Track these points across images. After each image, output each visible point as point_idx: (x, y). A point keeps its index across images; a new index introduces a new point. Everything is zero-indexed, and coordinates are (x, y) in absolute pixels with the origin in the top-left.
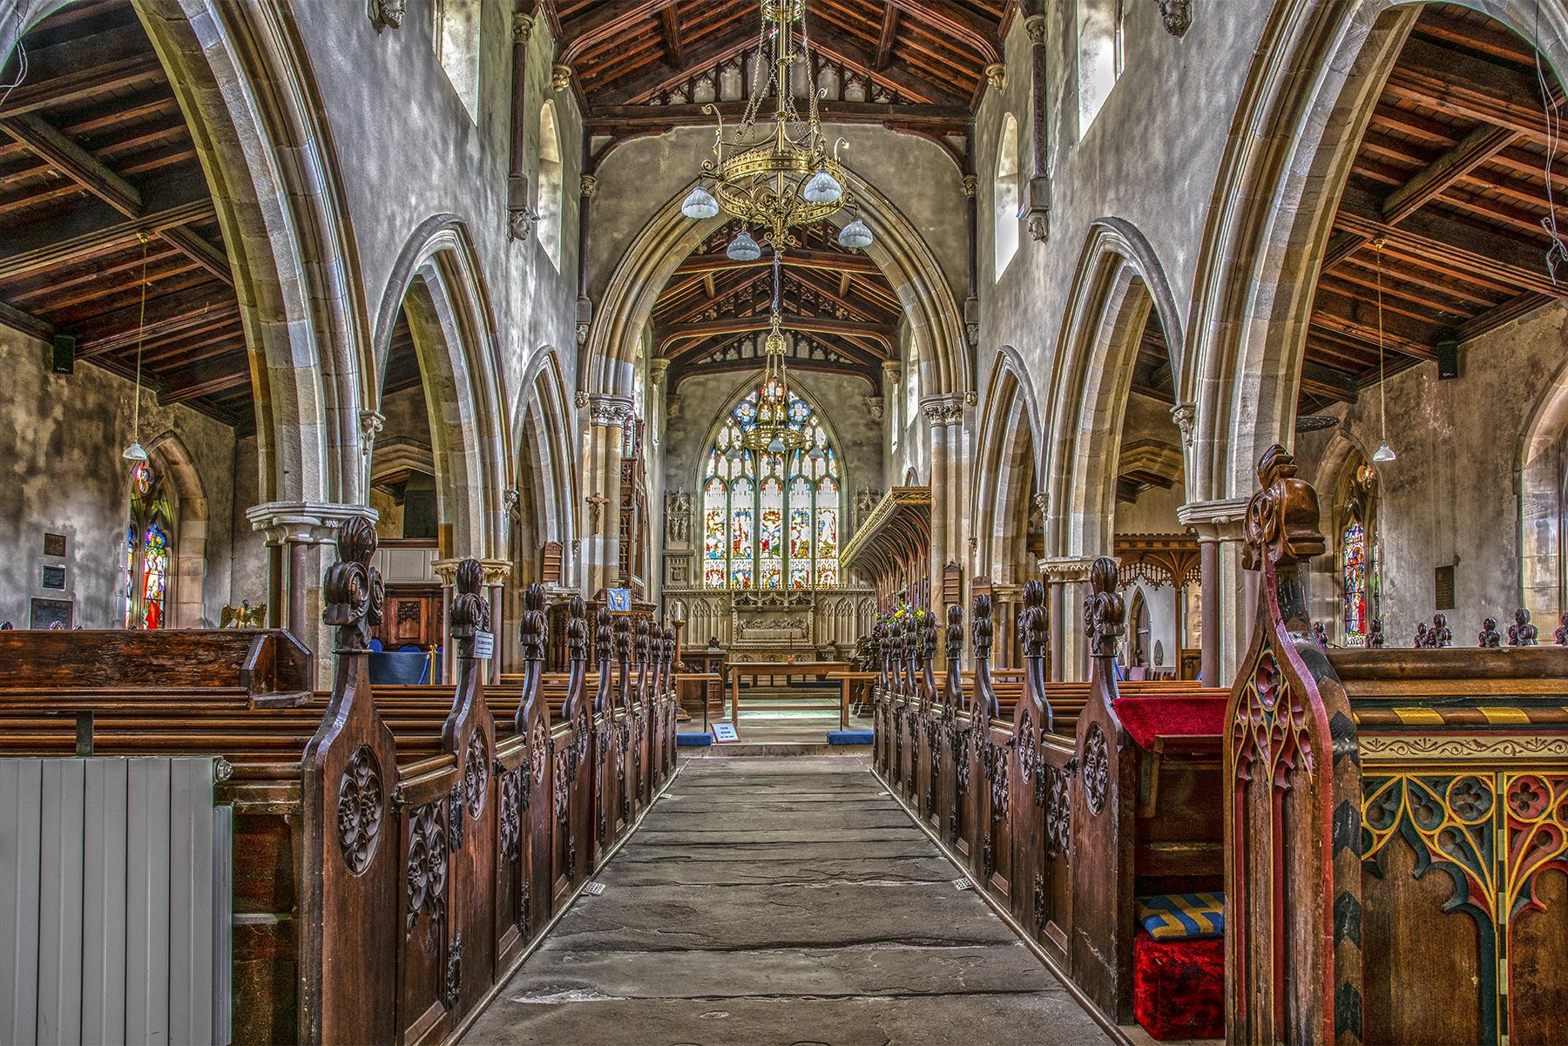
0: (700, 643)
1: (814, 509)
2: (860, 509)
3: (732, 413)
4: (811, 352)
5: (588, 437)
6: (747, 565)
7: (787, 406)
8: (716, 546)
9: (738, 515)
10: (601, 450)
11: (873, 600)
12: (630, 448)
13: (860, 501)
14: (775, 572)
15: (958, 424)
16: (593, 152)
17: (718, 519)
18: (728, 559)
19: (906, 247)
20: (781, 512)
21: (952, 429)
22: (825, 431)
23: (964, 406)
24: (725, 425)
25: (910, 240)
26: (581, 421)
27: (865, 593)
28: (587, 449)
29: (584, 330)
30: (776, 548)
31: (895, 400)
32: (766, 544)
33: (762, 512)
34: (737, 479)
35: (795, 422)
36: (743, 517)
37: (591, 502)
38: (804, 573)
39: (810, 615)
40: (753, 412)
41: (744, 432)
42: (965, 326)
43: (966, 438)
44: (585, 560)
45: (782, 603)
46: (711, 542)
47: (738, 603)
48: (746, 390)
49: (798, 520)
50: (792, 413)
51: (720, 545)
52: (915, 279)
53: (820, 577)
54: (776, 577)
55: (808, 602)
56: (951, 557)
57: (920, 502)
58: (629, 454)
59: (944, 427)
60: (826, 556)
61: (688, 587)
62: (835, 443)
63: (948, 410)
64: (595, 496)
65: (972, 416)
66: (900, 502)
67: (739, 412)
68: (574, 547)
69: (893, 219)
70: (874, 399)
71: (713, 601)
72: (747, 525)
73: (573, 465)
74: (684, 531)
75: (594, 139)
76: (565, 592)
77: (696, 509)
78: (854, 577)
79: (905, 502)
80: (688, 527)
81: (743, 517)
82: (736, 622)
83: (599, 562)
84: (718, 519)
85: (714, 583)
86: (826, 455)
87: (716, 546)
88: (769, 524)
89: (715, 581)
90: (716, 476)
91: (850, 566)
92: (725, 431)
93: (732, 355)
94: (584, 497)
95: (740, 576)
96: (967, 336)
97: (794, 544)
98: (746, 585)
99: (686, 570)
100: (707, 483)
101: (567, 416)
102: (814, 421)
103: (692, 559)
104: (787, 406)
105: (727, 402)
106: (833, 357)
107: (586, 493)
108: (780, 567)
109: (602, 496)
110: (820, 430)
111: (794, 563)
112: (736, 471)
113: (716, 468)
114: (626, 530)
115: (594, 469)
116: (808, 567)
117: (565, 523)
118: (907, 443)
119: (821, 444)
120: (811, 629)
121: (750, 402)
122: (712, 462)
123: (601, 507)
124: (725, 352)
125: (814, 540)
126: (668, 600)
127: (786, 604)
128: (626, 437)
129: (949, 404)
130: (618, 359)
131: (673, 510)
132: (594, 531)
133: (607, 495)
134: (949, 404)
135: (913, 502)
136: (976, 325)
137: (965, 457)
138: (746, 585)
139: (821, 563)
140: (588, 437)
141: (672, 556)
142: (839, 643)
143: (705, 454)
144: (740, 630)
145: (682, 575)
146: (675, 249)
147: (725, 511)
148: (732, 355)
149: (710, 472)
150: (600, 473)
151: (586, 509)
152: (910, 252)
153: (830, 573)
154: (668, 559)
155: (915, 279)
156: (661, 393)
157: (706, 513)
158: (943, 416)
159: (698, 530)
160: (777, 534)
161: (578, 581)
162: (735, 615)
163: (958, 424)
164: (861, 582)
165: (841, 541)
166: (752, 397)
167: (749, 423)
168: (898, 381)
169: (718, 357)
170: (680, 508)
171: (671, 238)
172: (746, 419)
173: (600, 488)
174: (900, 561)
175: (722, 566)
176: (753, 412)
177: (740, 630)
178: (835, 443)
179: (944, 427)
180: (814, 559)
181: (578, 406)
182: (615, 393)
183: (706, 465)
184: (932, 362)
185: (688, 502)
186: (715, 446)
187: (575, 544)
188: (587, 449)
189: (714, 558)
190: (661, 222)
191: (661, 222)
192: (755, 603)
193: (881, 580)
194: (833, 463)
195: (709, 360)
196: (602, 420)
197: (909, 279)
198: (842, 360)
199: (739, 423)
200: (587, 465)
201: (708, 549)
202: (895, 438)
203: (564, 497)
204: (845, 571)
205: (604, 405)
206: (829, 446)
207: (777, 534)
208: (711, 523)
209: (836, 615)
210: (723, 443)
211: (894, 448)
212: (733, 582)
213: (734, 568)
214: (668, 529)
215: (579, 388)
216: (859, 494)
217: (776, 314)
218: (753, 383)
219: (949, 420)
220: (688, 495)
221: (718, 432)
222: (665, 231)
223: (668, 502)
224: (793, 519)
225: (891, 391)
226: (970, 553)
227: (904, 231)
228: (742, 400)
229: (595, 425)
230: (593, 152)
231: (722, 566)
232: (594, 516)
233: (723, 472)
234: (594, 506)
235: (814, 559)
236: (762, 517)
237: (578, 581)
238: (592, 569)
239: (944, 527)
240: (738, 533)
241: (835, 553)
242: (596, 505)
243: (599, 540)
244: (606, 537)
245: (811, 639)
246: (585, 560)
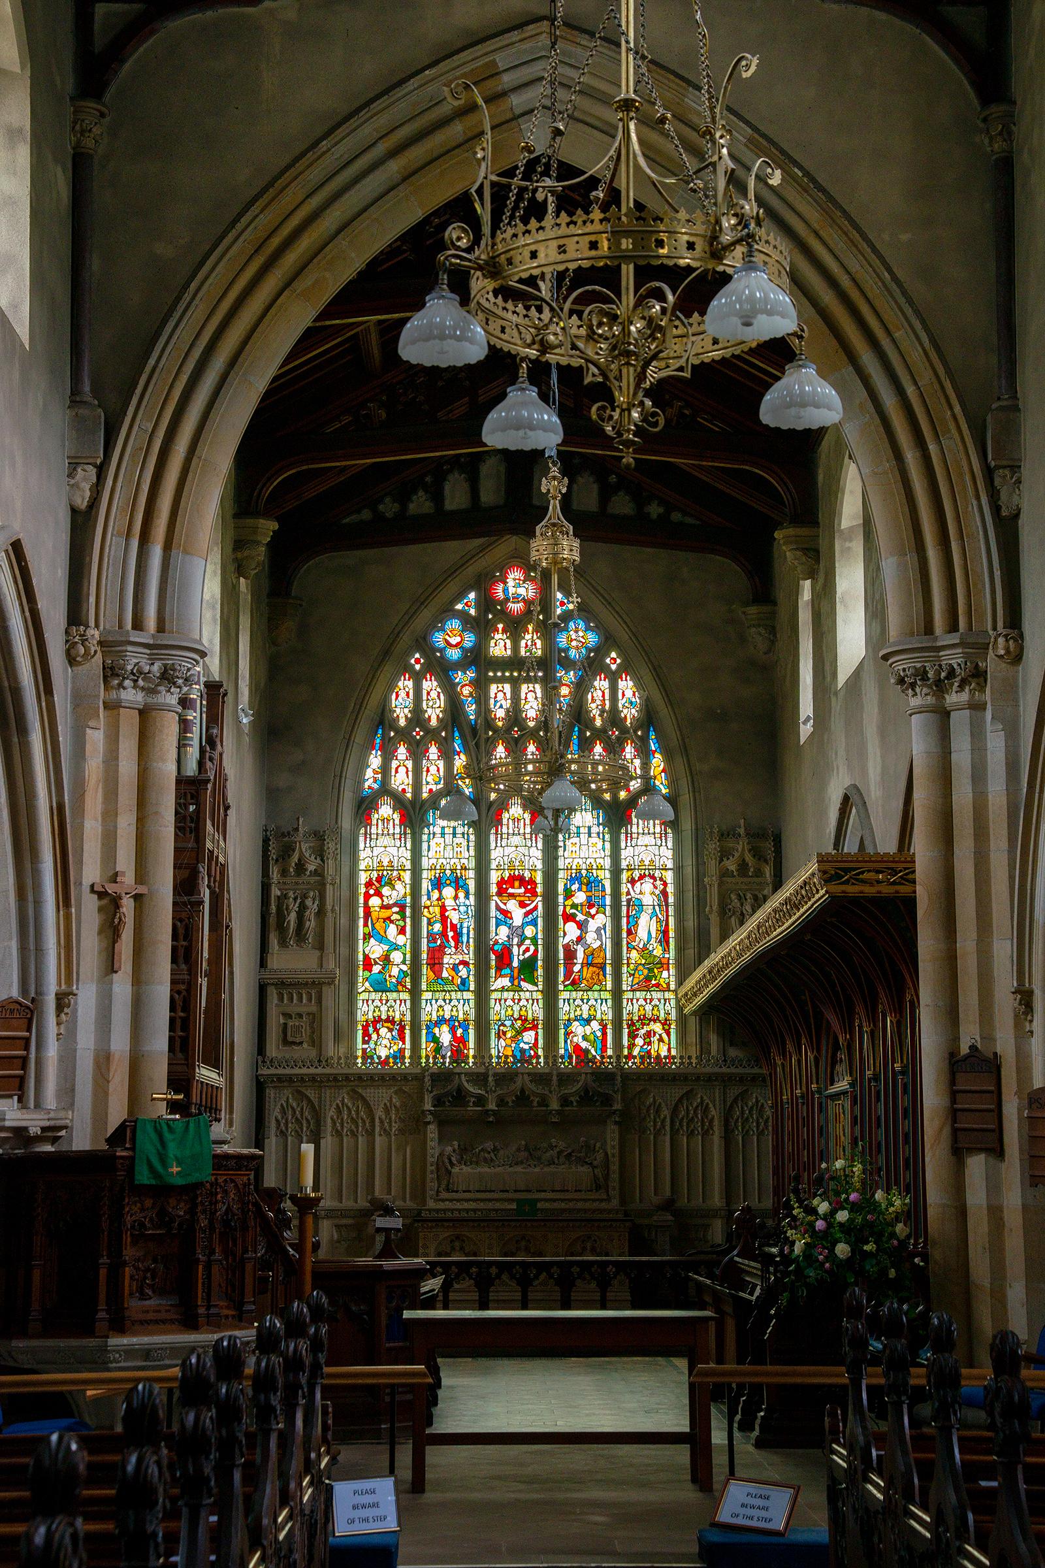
0: (348, 1203)
1: (616, 872)
2: (725, 874)
3: (423, 644)
4: (604, 498)
5: (96, 738)
6: (463, 1006)
7: (548, 630)
8: (386, 959)
9: (438, 884)
10: (128, 766)
11: (760, 1096)
12: (193, 752)
13: (724, 854)
14: (527, 1024)
15: (977, 707)
16: (99, 42)
17: (391, 894)
18: (415, 993)
19: (845, 282)
20: (539, 878)
21: (960, 721)
22: (639, 685)
23: (991, 664)
24: (407, 669)
25: (854, 265)
26: (79, 700)
27: (742, 1079)
28: (94, 766)
29: (86, 476)
30: (528, 966)
31: (805, 617)
32: (504, 957)
33: (494, 877)
34: (435, 797)
35: (567, 664)
36: (448, 892)
37: (102, 895)
38: (595, 1025)
39: (612, 1134)
40: (469, 640)
41: (449, 689)
42: (989, 473)
43: (996, 743)
44: (86, 1040)
45: (544, 1102)
46: (376, 950)
47: (438, 1101)
48: (452, 587)
49: (580, 897)
50: (562, 640)
51: (396, 957)
52: (868, 359)
53: (633, 1036)
54: (529, 1036)
55: (607, 1100)
56: (969, 1035)
57: (887, 890)
58: (191, 768)
59: (943, 715)
60: (646, 985)
61: (321, 1060)
62: (663, 711)
63: (951, 673)
64: (114, 878)
65: (1011, 691)
66: (837, 889)
67: (438, 639)
68: (60, 1008)
69: (813, 215)
70: (753, 610)
71: (380, 1097)
72: (461, 909)
73: (61, 807)
74: (311, 924)
75: (100, 9)
76: (34, 1122)
77: (338, 869)
78: (714, 1039)
79: (852, 889)
80: (321, 913)
81: (448, 892)
82: (433, 1147)
83: (120, 1043)
84: (391, 894)
85: (383, 1053)
86: (644, 740)
87: (386, 959)
88: (512, 905)
89: (384, 1046)
90: (385, 789)
91: (707, 1011)
92: (406, 684)
93: (420, 504)
94: (87, 881)
95: (446, 1038)
96: (994, 495)
97: (570, 955)
98: (458, 1055)
99: (315, 1020)
100: (365, 807)
101: (49, 690)
102: (613, 660)
103: (328, 992)
104: (548, 630)
105: (411, 615)
106: (654, 510)
107: (91, 872)
108: (536, 1011)
109: (129, 878)
110: (626, 686)
111: (569, 1003)
112: (432, 781)
113: (385, 769)
114: (183, 954)
115: (110, 815)
116: (605, 1011)
117: (40, 950)
118: (837, 725)
119: (629, 714)
120: (615, 1167)
121: (463, 616)
122: (375, 761)
123: (128, 906)
124: (403, 498)
125: (617, 945)
126: (270, 1093)
127: (555, 1105)
128: (185, 725)
129: (954, 658)
130: (168, 547)
131: (284, 873)
132: (110, 966)
133: (141, 875)
134: (954, 658)
135: (869, 890)
136: (1015, 468)
137: (997, 788)
138: (458, 1055)
139: (635, 1004)
140: (96, 738)
141: (282, 984)
142: (683, 1202)
143: (359, 737)
144: (443, 1170)
145: (305, 1035)
146: (300, 285)
147: (407, 876)
148: (420, 504)
149: (370, 779)
150: (126, 823)
151: (89, 910)
152: (855, 295)
153: (657, 1027)
154: (272, 993)
155: (868, 359)
156: (256, 594)
157: (363, 878)
158: (940, 687)
159: (344, 921)
160: (529, 931)
161: (68, 1091)
162: (432, 1131)
163: (977, 707)
164: (733, 1052)
165: (680, 949)
166: (469, 603)
167: (463, 665)
168: (812, 574)
169: (389, 508)
170: (300, 867)
171: (291, 259)
172: (454, 654)
173: (125, 862)
174: (831, 1017)
175: (400, 1009)
176: (469, 640)
177: (443, 1170)
178: (663, 711)
179: (943, 715)
180: (617, 993)
181: (71, 660)
182: (161, 628)
183: (363, 765)
184: (911, 559)
185: (320, 853)
186: (384, 719)
187: (63, 1001)
188: (94, 766)
189: (380, 987)
190: (265, 220)
191: (265, 220)
192: (480, 1100)
193: (784, 1053)
194: (657, 762)
195: (366, 515)
196: (131, 695)
197: (852, 358)
198: (676, 516)
199: (441, 668)
200: (94, 802)
201: (368, 964)
202: (806, 706)
203: (38, 886)
204: (693, 1024)
205: (134, 659)
206: (648, 718)
207: (529, 931)
208: (375, 902)
209: (674, 1133)
210: (401, 707)
211: (805, 730)
212: (426, 1047)
213: (429, 1011)
214: (272, 920)
215: (75, 616)
216: (723, 836)
217: (555, 471)
218: (471, 570)
219: (954, 698)
220: (319, 837)
221: (391, 686)
222: (276, 241)
223: (273, 854)
224: (569, 895)
225: (796, 592)
226: (1018, 1025)
227: (840, 245)
228: (447, 611)
229: (112, 706)
230: (99, 42)
231: (400, 1009)
232: (111, 929)
233: (401, 780)
234: (110, 903)
235: (617, 993)
236: (494, 889)
237: (68, 1091)
238: (103, 1060)
239: (951, 960)
240: (437, 927)
241: (668, 976)
242: (115, 902)
243: (122, 986)
244: (138, 979)
245: (615, 1193)
246: (86, 1040)
